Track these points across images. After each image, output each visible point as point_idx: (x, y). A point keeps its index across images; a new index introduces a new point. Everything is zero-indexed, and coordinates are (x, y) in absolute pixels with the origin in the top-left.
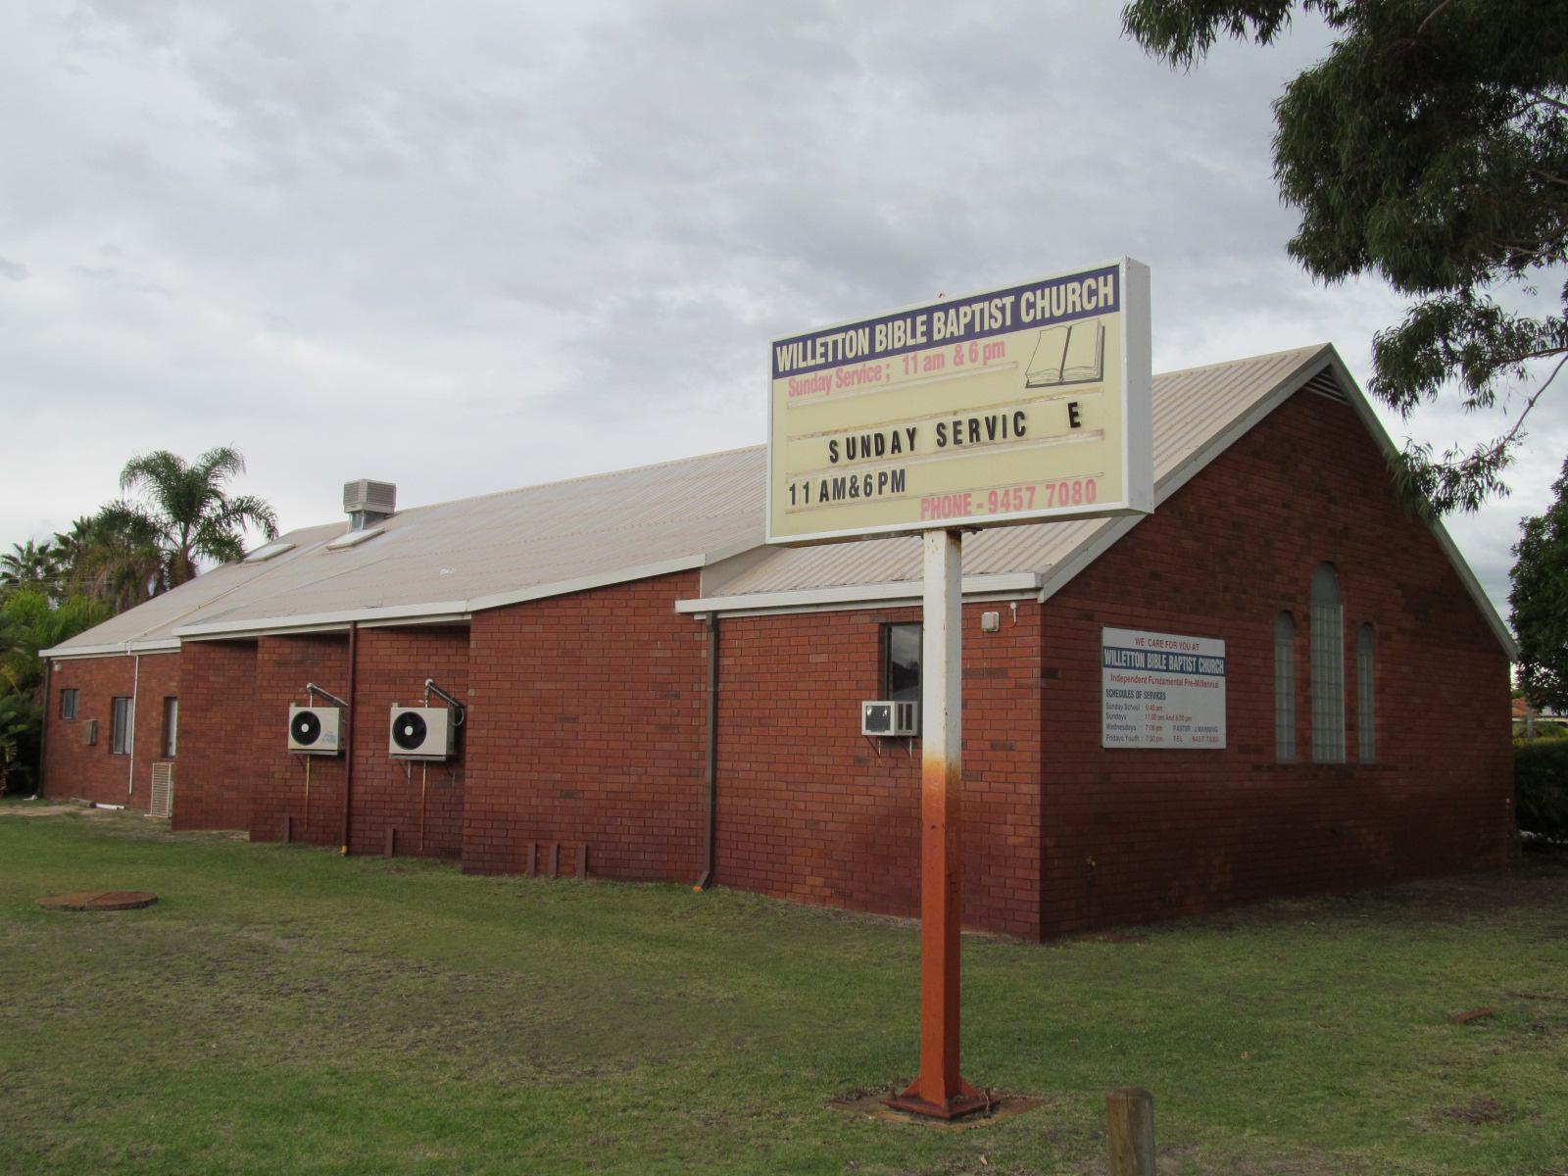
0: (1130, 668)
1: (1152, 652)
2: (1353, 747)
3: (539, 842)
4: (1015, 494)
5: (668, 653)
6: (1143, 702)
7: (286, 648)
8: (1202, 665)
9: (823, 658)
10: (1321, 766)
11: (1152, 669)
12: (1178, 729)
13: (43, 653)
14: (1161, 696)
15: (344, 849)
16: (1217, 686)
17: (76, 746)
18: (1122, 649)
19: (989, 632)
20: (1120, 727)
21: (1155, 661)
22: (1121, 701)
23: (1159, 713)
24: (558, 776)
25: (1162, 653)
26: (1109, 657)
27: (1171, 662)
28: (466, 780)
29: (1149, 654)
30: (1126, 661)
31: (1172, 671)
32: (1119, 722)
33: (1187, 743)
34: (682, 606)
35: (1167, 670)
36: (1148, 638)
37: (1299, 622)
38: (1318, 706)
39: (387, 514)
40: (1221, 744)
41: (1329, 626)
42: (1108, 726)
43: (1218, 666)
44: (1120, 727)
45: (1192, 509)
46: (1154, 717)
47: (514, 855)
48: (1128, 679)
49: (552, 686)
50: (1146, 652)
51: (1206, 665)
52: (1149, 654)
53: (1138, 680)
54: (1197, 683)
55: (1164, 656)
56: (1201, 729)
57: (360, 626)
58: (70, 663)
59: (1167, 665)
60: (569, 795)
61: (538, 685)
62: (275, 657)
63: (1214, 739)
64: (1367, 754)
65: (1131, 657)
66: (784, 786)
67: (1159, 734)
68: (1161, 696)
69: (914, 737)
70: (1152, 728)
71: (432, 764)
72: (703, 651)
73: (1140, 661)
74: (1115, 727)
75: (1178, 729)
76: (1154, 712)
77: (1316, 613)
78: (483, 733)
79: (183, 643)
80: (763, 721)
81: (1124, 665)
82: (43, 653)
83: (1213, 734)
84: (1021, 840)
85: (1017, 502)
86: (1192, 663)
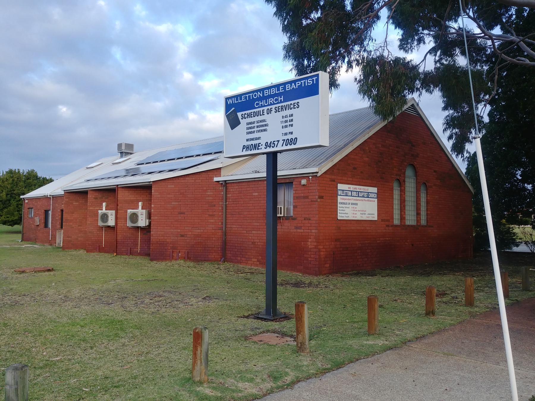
0: (347, 196)
1: (353, 191)
2: (418, 220)
3: (174, 250)
4: (273, 142)
5: (212, 193)
6: (350, 206)
7: (97, 194)
8: (370, 195)
9: (256, 194)
10: (409, 226)
11: (353, 196)
12: (362, 214)
13: (22, 197)
14: (356, 204)
15: (115, 254)
16: (374, 201)
17: (33, 225)
18: (344, 190)
19: (304, 185)
20: (343, 213)
21: (354, 194)
22: (344, 206)
23: (355, 209)
24: (179, 231)
25: (357, 191)
26: (340, 193)
27: (359, 194)
28: (151, 232)
29: (352, 192)
30: (345, 194)
31: (360, 197)
32: (343, 212)
33: (365, 218)
34: (216, 179)
35: (358, 197)
36: (352, 187)
37: (402, 184)
38: (407, 208)
39: (131, 153)
40: (376, 219)
41: (410, 185)
42: (339, 213)
43: (375, 195)
44: (343, 213)
45: (367, 148)
46: (354, 210)
47: (166, 254)
48: (346, 199)
49: (177, 203)
50: (352, 191)
51: (371, 195)
52: (352, 192)
53: (349, 199)
54: (368, 201)
55: (357, 192)
56: (369, 214)
57: (119, 186)
58: (31, 199)
59: (358, 195)
60: (182, 236)
61: (173, 203)
62: (93, 196)
63: (374, 217)
64: (423, 222)
65: (347, 192)
66: (245, 232)
67: (356, 216)
68: (356, 204)
69: (282, 217)
70: (353, 214)
71: (142, 229)
72: (222, 192)
73: (350, 194)
74: (342, 213)
75: (362, 214)
76: (354, 209)
77: (407, 180)
78: (156, 218)
79: (64, 192)
80: (239, 213)
81: (345, 195)
82: (22, 197)
83: (373, 216)
84: (313, 246)
85: (273, 145)
86: (366, 194)
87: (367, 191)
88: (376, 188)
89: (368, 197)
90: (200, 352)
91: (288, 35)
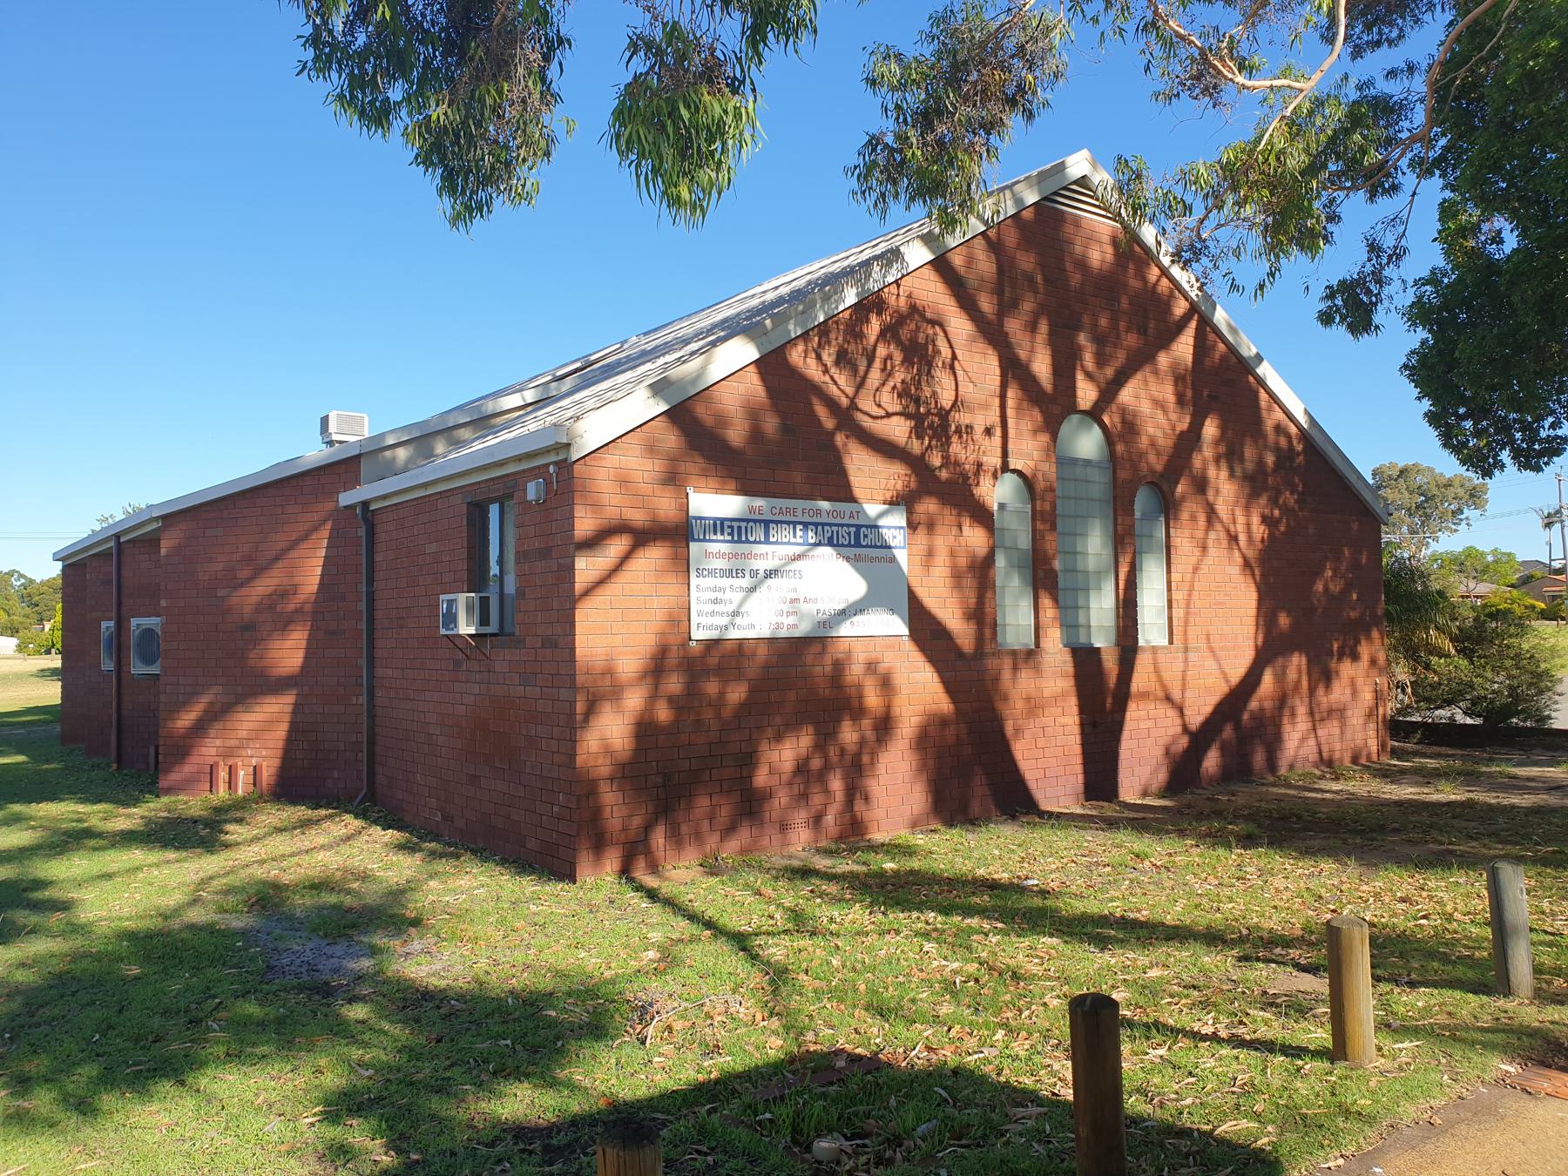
86: (849, 534)
87: (852, 522)
88: (1085, 150)
89: (860, 546)
90: (1334, 788)
91: (713, 105)
